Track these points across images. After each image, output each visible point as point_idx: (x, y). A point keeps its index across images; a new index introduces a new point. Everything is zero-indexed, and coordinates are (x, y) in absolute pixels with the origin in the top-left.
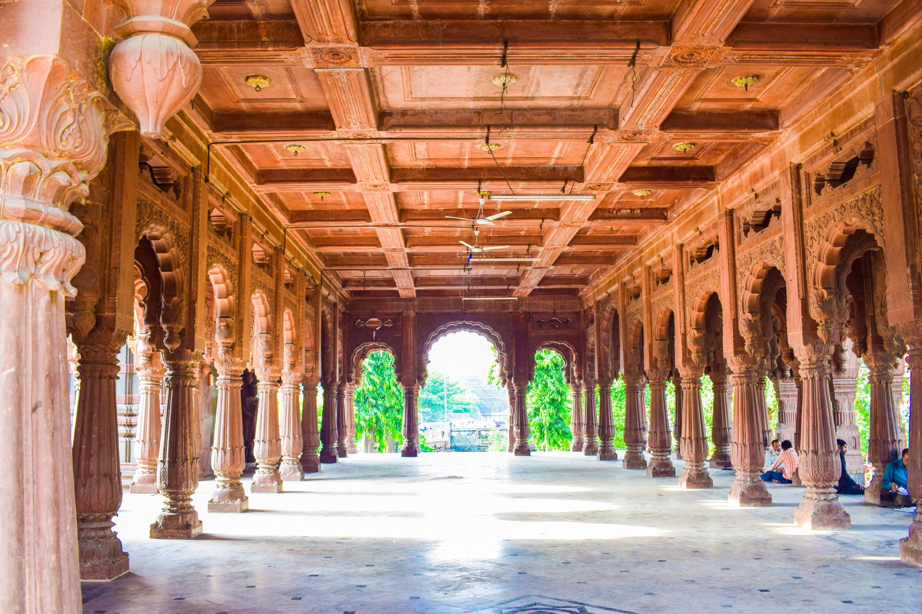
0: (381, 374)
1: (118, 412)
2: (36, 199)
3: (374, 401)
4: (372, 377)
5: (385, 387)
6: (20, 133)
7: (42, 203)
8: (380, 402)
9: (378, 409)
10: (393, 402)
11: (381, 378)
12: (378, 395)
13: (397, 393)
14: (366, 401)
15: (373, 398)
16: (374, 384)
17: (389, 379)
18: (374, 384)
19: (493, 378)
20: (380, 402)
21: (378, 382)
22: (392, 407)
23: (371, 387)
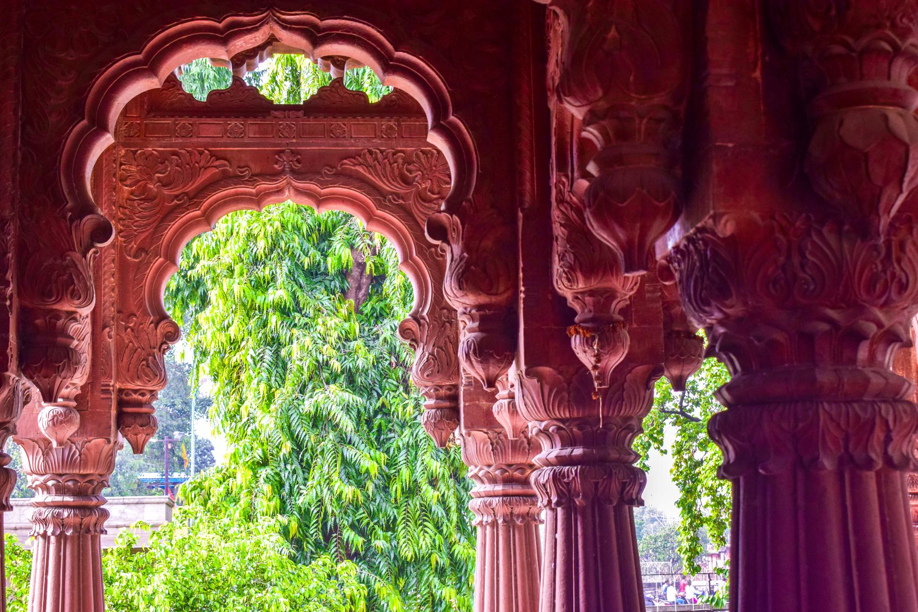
0: (380, 443)
1: (5, 525)
2: (119, 238)
3: (359, 541)
4: (349, 452)
5: (396, 488)
6: (421, 209)
7: (480, 243)
8: (380, 543)
9: (372, 567)
10: (425, 543)
11: (383, 457)
12: (372, 515)
13: (438, 510)
14: (327, 538)
15: (353, 527)
16: (354, 475)
17: (411, 463)
18: (354, 475)
19: (369, 78)
20: (380, 543)
21: (374, 470)
22: (419, 561)
23: (349, 491)
